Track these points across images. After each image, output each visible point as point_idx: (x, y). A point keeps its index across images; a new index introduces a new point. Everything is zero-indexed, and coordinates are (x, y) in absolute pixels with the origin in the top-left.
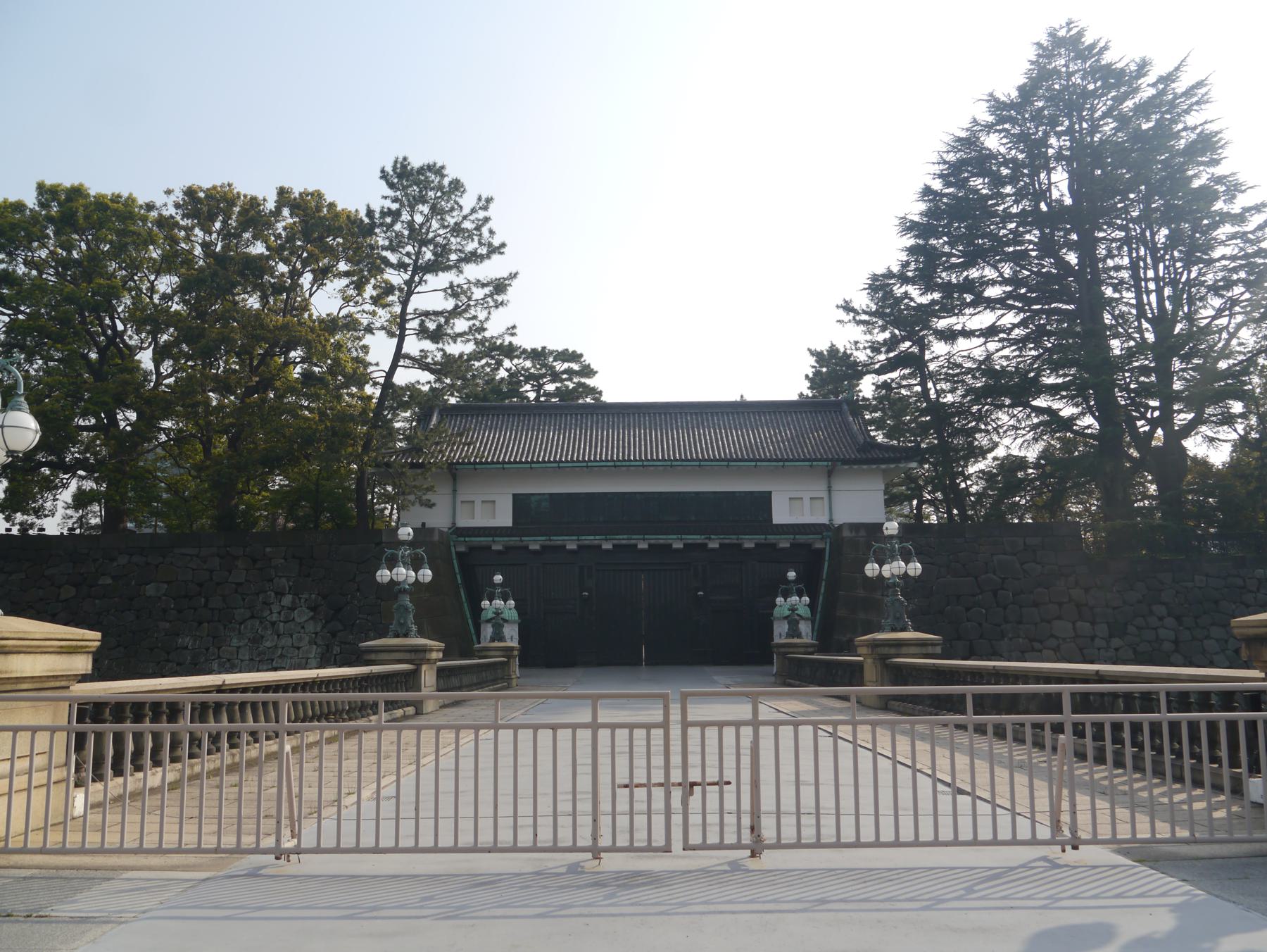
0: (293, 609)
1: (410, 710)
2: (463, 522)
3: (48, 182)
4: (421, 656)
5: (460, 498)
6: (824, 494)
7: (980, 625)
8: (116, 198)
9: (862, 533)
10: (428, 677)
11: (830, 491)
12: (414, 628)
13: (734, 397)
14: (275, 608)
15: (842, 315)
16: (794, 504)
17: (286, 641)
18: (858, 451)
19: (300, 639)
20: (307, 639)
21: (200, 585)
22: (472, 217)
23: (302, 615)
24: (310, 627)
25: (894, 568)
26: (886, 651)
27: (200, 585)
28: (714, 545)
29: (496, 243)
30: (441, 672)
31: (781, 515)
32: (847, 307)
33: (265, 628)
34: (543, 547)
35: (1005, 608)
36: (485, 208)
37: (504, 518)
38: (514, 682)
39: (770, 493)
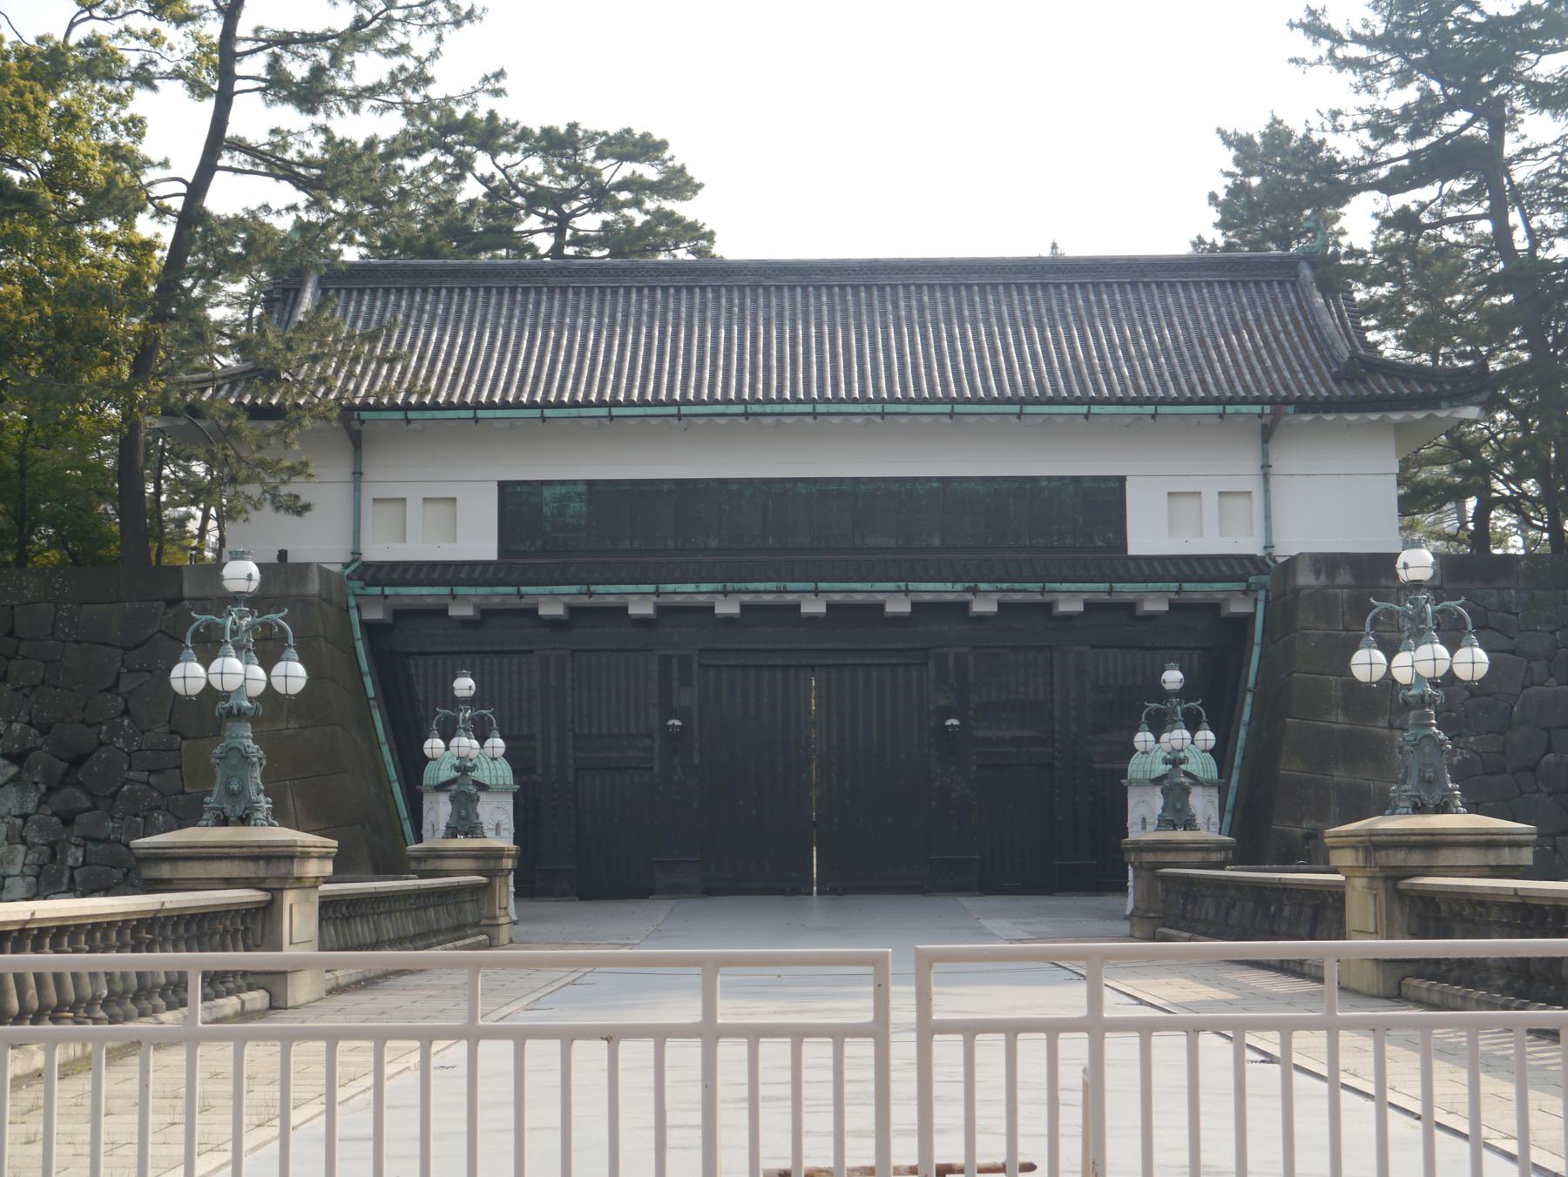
1: (257, 999)
2: (378, 550)
4: (281, 869)
5: (370, 491)
6: (1253, 484)
9: (1344, 578)
10: (299, 917)
11: (1266, 476)
12: (265, 803)
13: (1046, 252)
16: (1184, 507)
18: (1336, 379)
25: (1420, 662)
26: (1399, 858)
30: (329, 907)
31: (1147, 534)
34: (576, 612)
37: (479, 541)
38: (504, 934)
39: (1122, 480)
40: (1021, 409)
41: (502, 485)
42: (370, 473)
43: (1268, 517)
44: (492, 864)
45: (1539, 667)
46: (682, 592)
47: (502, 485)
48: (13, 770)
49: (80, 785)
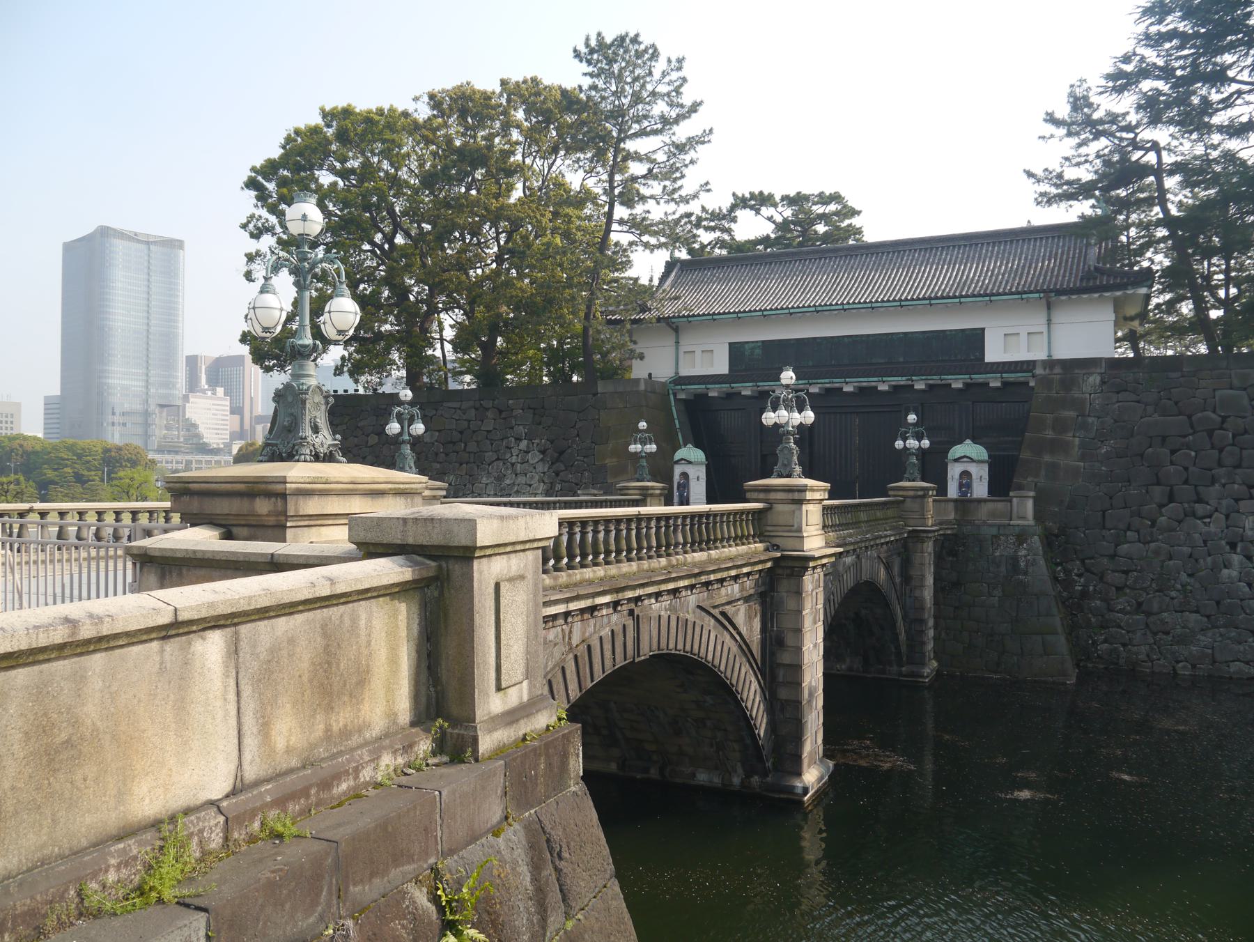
0: (527, 452)
2: (684, 372)
3: (328, 109)
5: (682, 349)
6: (1044, 329)
7: (1186, 469)
8: (380, 112)
9: (1058, 370)
11: (1049, 324)
12: (798, 469)
13: (1024, 225)
14: (515, 452)
15: (1050, 129)
16: (1011, 341)
17: (521, 479)
19: (532, 478)
20: (537, 477)
21: (461, 433)
22: (666, 80)
23: (534, 457)
24: (540, 468)
27: (461, 433)
28: (920, 386)
29: (687, 100)
31: (994, 353)
32: (1051, 119)
33: (507, 469)
34: (967, 385)
35: (1221, 451)
36: (679, 69)
39: (983, 330)
42: (682, 342)
43: (1049, 343)
44: (796, 496)
45: (1150, 409)
46: (865, 382)
47: (732, 346)
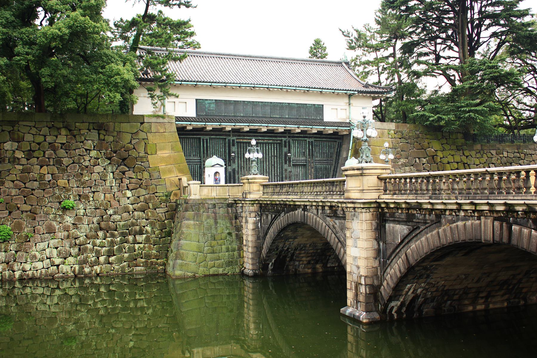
16: (334, 112)
31: (329, 116)
37: (192, 113)
39: (323, 105)
40: (307, 91)
41: (197, 100)
47: (197, 100)
48: (109, 162)
49: (125, 165)
